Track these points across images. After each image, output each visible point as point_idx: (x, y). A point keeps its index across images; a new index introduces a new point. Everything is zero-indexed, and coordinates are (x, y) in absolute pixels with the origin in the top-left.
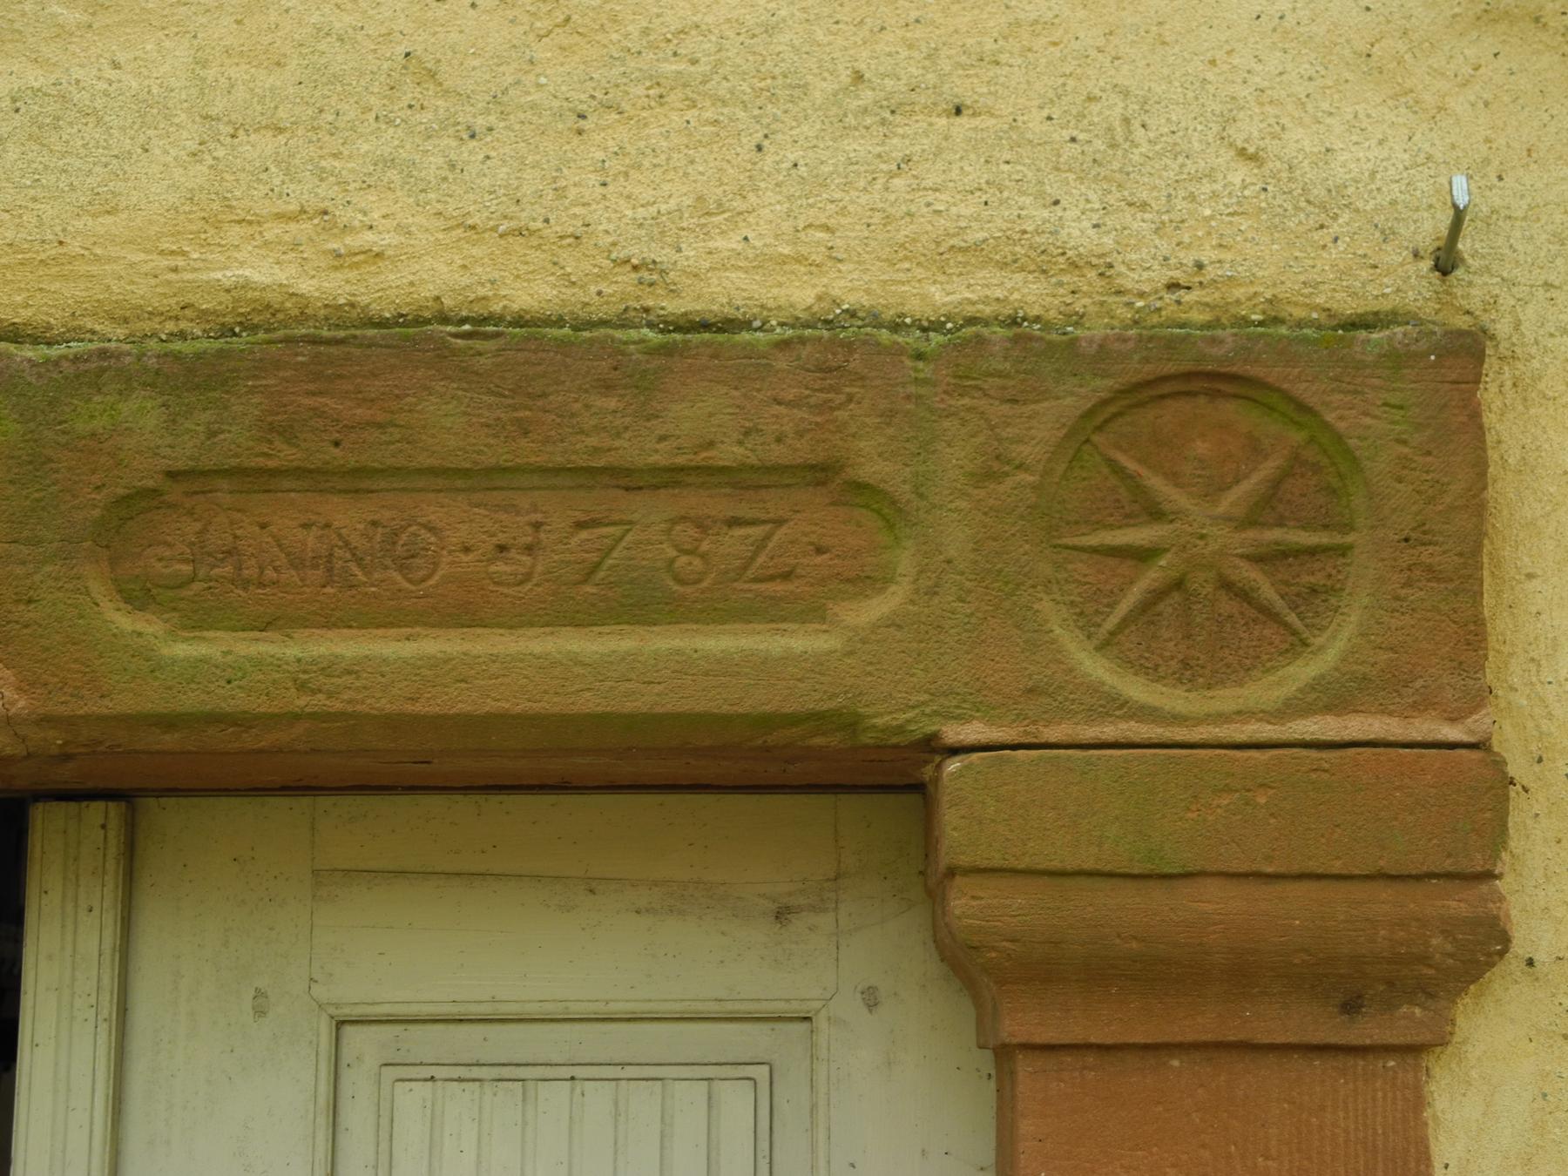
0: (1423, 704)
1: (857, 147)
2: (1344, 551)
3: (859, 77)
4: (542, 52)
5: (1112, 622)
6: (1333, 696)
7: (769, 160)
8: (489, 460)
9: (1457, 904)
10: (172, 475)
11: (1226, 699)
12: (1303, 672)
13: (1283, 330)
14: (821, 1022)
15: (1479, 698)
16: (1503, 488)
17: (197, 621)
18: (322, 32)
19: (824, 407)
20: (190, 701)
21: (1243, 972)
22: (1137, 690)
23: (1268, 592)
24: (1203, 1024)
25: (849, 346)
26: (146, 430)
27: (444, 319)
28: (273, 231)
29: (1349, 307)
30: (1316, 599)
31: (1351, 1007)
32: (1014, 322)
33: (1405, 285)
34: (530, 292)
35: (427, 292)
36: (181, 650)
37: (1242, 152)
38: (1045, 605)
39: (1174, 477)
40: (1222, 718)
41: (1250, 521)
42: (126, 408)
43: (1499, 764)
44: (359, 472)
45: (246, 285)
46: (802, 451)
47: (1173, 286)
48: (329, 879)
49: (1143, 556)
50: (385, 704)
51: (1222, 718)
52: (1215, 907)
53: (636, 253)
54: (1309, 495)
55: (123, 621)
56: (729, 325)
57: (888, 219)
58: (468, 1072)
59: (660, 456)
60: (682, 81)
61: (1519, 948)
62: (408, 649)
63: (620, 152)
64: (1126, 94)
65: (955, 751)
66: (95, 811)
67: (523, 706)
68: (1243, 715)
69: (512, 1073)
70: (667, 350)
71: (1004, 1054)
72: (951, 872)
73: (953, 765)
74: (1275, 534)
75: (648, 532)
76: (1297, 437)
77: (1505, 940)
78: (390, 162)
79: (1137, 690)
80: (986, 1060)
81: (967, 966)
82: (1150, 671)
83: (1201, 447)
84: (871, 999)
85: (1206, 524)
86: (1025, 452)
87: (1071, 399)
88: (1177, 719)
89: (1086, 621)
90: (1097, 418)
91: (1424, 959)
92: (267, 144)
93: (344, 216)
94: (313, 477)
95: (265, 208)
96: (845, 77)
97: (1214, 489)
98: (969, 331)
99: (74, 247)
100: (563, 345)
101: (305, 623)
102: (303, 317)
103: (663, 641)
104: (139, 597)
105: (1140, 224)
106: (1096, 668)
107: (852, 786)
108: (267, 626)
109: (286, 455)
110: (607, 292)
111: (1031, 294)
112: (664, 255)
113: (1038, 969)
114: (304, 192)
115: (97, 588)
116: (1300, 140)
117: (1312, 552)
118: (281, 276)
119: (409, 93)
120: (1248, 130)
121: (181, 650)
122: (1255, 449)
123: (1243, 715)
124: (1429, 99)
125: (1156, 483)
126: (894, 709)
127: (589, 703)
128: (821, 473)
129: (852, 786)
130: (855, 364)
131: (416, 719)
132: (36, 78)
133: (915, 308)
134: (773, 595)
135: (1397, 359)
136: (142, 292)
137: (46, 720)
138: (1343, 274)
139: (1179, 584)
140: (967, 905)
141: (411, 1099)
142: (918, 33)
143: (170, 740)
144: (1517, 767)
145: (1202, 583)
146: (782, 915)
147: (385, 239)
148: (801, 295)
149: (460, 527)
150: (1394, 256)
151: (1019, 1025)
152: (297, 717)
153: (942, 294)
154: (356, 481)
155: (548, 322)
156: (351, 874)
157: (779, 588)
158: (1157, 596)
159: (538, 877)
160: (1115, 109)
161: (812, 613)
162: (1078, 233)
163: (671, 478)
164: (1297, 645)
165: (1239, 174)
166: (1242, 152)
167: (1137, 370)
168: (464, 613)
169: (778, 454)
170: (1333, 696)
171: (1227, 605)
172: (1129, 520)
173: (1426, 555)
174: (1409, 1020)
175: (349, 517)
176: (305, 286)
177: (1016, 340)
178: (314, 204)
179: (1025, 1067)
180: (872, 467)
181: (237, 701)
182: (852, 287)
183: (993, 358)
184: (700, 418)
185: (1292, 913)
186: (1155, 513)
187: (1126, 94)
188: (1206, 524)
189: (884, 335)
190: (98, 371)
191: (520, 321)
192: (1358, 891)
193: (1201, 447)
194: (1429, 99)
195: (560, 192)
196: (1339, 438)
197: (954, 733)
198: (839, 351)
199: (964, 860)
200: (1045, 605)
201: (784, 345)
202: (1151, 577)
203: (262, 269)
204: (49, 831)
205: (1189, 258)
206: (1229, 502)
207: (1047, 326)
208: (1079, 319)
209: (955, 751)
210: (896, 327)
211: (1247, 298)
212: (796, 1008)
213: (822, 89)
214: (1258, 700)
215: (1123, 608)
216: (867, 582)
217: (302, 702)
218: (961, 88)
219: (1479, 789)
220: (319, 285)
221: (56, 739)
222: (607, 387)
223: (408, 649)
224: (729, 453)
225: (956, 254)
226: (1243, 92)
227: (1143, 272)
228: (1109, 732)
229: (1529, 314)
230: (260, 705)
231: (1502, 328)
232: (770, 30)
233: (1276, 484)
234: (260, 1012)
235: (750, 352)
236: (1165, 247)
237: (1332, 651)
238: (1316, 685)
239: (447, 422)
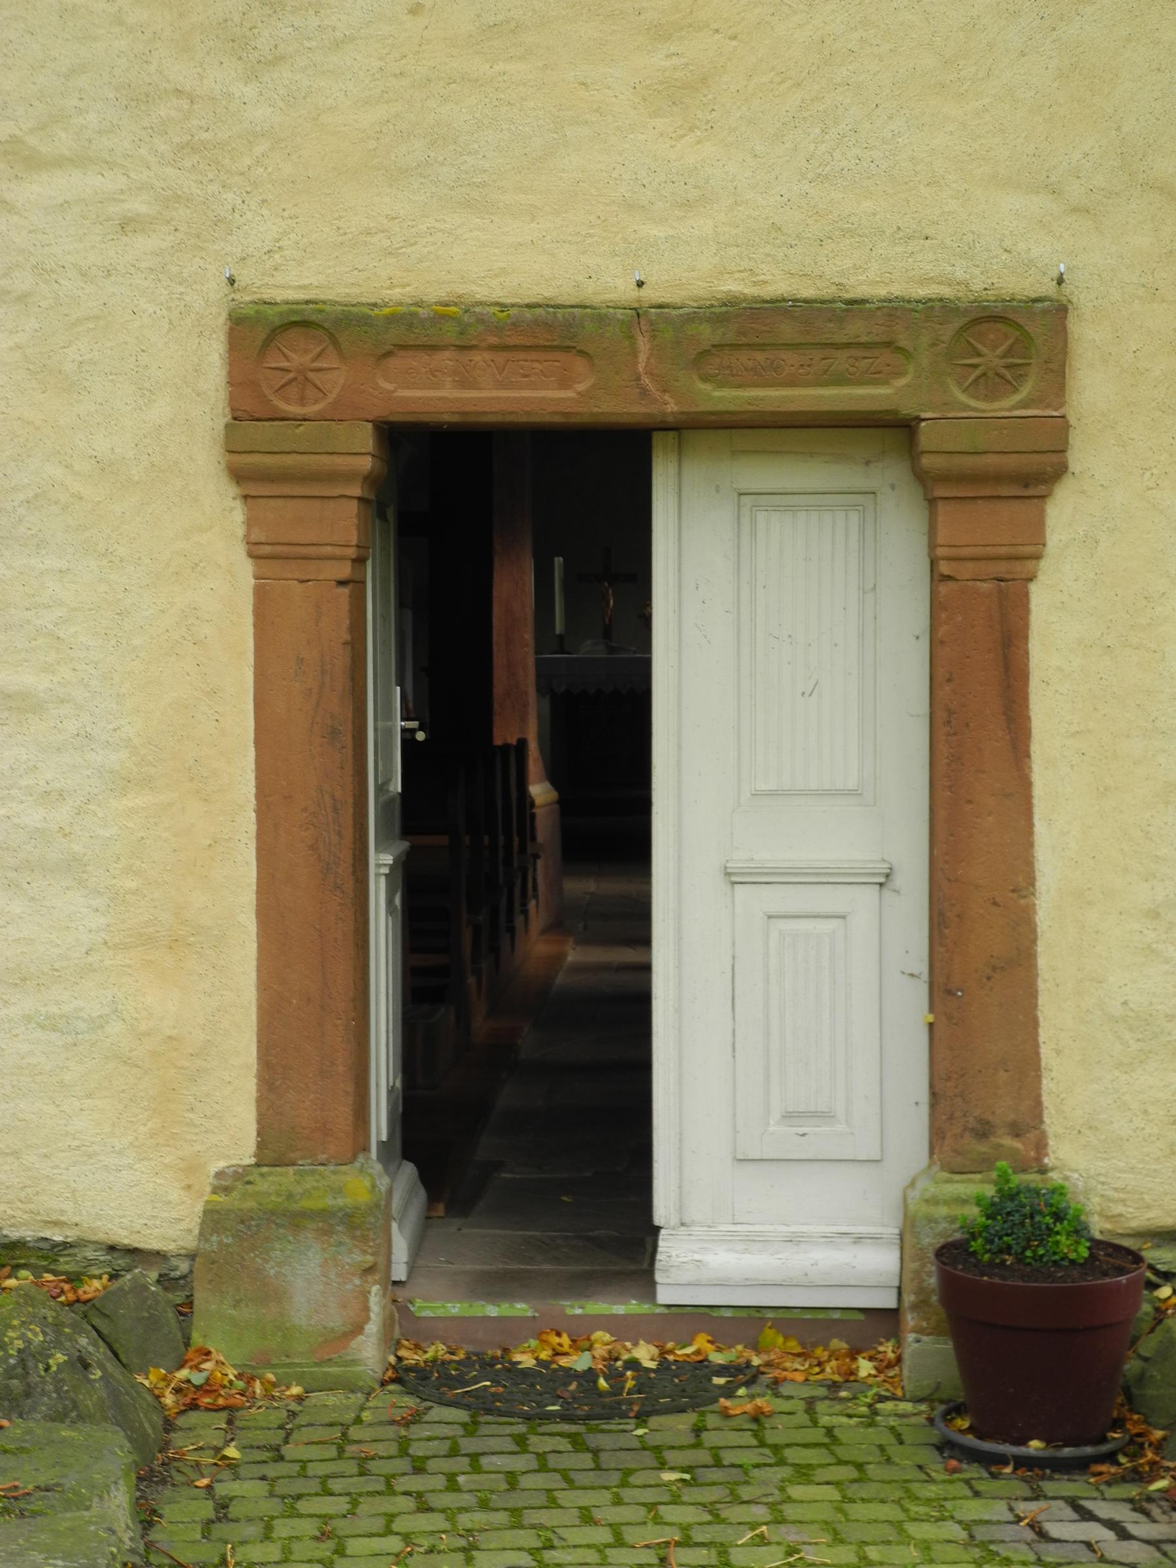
0: (1048, 406)
1: (899, 249)
2: (1029, 364)
3: (899, 228)
4: (809, 221)
5: (966, 384)
6: (1024, 405)
7: (873, 254)
8: (798, 341)
9: (1054, 458)
10: (713, 346)
11: (996, 405)
12: (1017, 398)
13: (1015, 303)
14: (878, 494)
15: (1062, 404)
16: (1073, 345)
17: (721, 385)
18: (749, 217)
19: (888, 326)
20: (720, 407)
21: (998, 478)
22: (973, 403)
23: (1009, 376)
24: (987, 492)
25: (896, 309)
26: (706, 334)
27: (784, 300)
28: (737, 275)
29: (1034, 295)
30: (1021, 378)
31: (1026, 486)
32: (941, 300)
33: (1048, 288)
34: (808, 292)
35: (780, 292)
36: (717, 394)
37: (1006, 250)
38: (949, 380)
39: (984, 344)
40: (995, 411)
41: (1004, 356)
42: (701, 328)
43: (1067, 422)
44: (764, 345)
45: (730, 291)
46: (884, 338)
47: (986, 289)
48: (736, 453)
49: (975, 366)
50: (772, 409)
51: (995, 411)
52: (992, 461)
53: (837, 280)
54: (1022, 345)
55: (702, 386)
56: (863, 301)
57: (907, 270)
58: (777, 508)
59: (845, 340)
60: (849, 230)
61: (1071, 469)
62: (777, 393)
63: (833, 251)
64: (973, 233)
65: (924, 420)
66: (672, 434)
67: (808, 409)
68: (1001, 410)
69: (788, 508)
70: (847, 310)
71: (932, 502)
72: (922, 452)
73: (923, 424)
74: (1011, 360)
75: (841, 361)
76: (1018, 333)
77: (1066, 468)
78: (769, 255)
79: (973, 403)
80: (925, 504)
81: (922, 478)
82: (977, 398)
83: (992, 336)
84: (893, 487)
85: (992, 358)
86: (945, 338)
87: (957, 323)
88: (984, 411)
89: (959, 384)
90: (964, 328)
91: (1045, 473)
92: (735, 250)
93: (757, 271)
94: (750, 346)
95: (735, 269)
96: (895, 228)
97: (995, 348)
98: (929, 304)
99: (684, 281)
100: (819, 309)
101: (749, 386)
102: (745, 300)
103: (846, 391)
104: (705, 379)
105: (977, 271)
106: (963, 398)
107: (896, 431)
108: (739, 386)
109: (744, 340)
110: (828, 292)
111: (946, 291)
112: (844, 281)
113: (946, 478)
114: (745, 264)
115: (695, 377)
116: (1022, 246)
117: (1021, 365)
118: (740, 288)
119: (774, 235)
120: (1007, 243)
121: (717, 394)
122: (1006, 337)
123: (1001, 410)
124: (1058, 234)
125: (979, 346)
126: (907, 408)
127: (826, 408)
128: (888, 344)
129: (896, 431)
130: (899, 313)
131: (780, 413)
132: (671, 232)
133: (914, 296)
134: (876, 377)
135: (1045, 312)
136: (702, 293)
137: (682, 413)
138: (1032, 285)
139: (984, 374)
140: (926, 461)
141: (761, 516)
142: (916, 215)
143: (713, 418)
144: (1072, 421)
145: (991, 374)
146: (867, 463)
147: (768, 277)
148: (882, 292)
149: (790, 359)
150: (1046, 280)
151: (939, 492)
152: (747, 412)
153: (922, 292)
154: (762, 347)
155: (815, 301)
156: (743, 452)
157: (877, 376)
158: (979, 378)
159: (796, 453)
160: (971, 237)
161: (886, 383)
162: (960, 274)
163: (847, 346)
164: (1016, 390)
165: (1005, 256)
166: (1006, 250)
167: (974, 315)
168: (791, 383)
169: (877, 339)
170: (1024, 405)
171: (997, 380)
172: (972, 356)
173: (1050, 366)
174: (1041, 489)
175: (760, 356)
176: (746, 291)
177: (943, 307)
178: (748, 267)
179: (940, 504)
180: (903, 343)
181: (732, 408)
182: (896, 290)
183: (936, 310)
184: (856, 329)
185: (1011, 462)
186: (979, 355)
187: (973, 233)
188: (992, 358)
189: (907, 305)
190: (692, 318)
191: (806, 301)
192: (1029, 456)
193: (992, 336)
194: (1058, 234)
195: (816, 263)
196: (1028, 334)
197: (924, 415)
198: (895, 310)
199: (926, 449)
200: (949, 380)
201: (879, 308)
202: (978, 372)
203: (735, 286)
204: (658, 439)
205: (990, 281)
206: (999, 351)
207: (951, 301)
208: (959, 299)
209: (924, 420)
210: (909, 301)
211: (1006, 293)
212: (872, 490)
213: (889, 232)
214: (1006, 405)
215: (970, 381)
216: (899, 374)
217: (750, 408)
218: (928, 231)
219: (1061, 427)
220: (750, 291)
221: (684, 417)
222: (831, 321)
223: (777, 393)
224: (864, 339)
225: (926, 280)
226: (1007, 232)
227: (977, 286)
228: (965, 414)
229: (1082, 297)
230: (738, 409)
231: (1075, 300)
232: (874, 214)
233: (1011, 346)
234: (717, 491)
235: (870, 310)
236: (983, 278)
237: (1024, 392)
238: (1021, 401)
239: (787, 331)
